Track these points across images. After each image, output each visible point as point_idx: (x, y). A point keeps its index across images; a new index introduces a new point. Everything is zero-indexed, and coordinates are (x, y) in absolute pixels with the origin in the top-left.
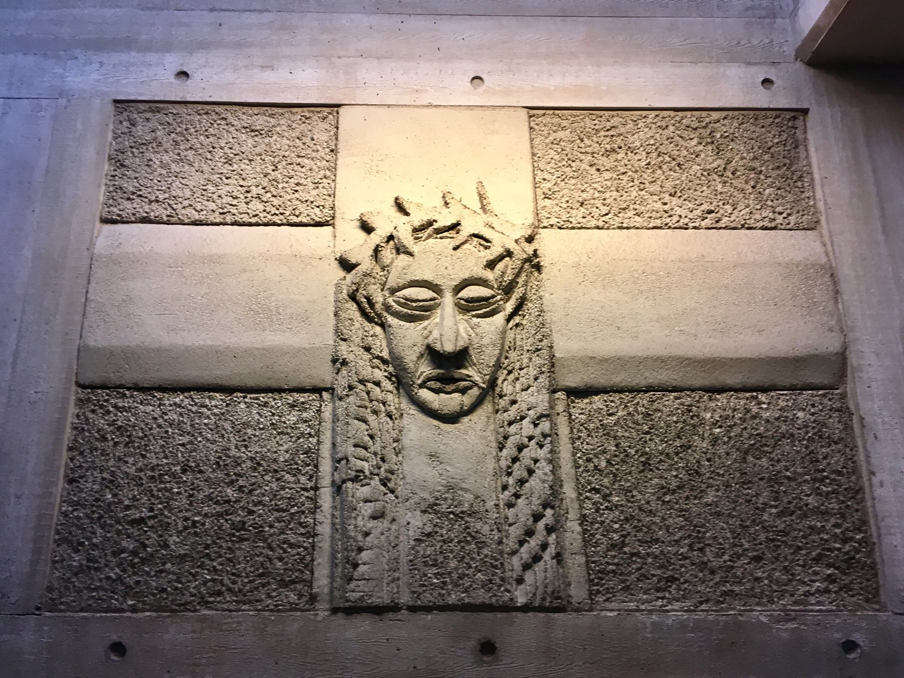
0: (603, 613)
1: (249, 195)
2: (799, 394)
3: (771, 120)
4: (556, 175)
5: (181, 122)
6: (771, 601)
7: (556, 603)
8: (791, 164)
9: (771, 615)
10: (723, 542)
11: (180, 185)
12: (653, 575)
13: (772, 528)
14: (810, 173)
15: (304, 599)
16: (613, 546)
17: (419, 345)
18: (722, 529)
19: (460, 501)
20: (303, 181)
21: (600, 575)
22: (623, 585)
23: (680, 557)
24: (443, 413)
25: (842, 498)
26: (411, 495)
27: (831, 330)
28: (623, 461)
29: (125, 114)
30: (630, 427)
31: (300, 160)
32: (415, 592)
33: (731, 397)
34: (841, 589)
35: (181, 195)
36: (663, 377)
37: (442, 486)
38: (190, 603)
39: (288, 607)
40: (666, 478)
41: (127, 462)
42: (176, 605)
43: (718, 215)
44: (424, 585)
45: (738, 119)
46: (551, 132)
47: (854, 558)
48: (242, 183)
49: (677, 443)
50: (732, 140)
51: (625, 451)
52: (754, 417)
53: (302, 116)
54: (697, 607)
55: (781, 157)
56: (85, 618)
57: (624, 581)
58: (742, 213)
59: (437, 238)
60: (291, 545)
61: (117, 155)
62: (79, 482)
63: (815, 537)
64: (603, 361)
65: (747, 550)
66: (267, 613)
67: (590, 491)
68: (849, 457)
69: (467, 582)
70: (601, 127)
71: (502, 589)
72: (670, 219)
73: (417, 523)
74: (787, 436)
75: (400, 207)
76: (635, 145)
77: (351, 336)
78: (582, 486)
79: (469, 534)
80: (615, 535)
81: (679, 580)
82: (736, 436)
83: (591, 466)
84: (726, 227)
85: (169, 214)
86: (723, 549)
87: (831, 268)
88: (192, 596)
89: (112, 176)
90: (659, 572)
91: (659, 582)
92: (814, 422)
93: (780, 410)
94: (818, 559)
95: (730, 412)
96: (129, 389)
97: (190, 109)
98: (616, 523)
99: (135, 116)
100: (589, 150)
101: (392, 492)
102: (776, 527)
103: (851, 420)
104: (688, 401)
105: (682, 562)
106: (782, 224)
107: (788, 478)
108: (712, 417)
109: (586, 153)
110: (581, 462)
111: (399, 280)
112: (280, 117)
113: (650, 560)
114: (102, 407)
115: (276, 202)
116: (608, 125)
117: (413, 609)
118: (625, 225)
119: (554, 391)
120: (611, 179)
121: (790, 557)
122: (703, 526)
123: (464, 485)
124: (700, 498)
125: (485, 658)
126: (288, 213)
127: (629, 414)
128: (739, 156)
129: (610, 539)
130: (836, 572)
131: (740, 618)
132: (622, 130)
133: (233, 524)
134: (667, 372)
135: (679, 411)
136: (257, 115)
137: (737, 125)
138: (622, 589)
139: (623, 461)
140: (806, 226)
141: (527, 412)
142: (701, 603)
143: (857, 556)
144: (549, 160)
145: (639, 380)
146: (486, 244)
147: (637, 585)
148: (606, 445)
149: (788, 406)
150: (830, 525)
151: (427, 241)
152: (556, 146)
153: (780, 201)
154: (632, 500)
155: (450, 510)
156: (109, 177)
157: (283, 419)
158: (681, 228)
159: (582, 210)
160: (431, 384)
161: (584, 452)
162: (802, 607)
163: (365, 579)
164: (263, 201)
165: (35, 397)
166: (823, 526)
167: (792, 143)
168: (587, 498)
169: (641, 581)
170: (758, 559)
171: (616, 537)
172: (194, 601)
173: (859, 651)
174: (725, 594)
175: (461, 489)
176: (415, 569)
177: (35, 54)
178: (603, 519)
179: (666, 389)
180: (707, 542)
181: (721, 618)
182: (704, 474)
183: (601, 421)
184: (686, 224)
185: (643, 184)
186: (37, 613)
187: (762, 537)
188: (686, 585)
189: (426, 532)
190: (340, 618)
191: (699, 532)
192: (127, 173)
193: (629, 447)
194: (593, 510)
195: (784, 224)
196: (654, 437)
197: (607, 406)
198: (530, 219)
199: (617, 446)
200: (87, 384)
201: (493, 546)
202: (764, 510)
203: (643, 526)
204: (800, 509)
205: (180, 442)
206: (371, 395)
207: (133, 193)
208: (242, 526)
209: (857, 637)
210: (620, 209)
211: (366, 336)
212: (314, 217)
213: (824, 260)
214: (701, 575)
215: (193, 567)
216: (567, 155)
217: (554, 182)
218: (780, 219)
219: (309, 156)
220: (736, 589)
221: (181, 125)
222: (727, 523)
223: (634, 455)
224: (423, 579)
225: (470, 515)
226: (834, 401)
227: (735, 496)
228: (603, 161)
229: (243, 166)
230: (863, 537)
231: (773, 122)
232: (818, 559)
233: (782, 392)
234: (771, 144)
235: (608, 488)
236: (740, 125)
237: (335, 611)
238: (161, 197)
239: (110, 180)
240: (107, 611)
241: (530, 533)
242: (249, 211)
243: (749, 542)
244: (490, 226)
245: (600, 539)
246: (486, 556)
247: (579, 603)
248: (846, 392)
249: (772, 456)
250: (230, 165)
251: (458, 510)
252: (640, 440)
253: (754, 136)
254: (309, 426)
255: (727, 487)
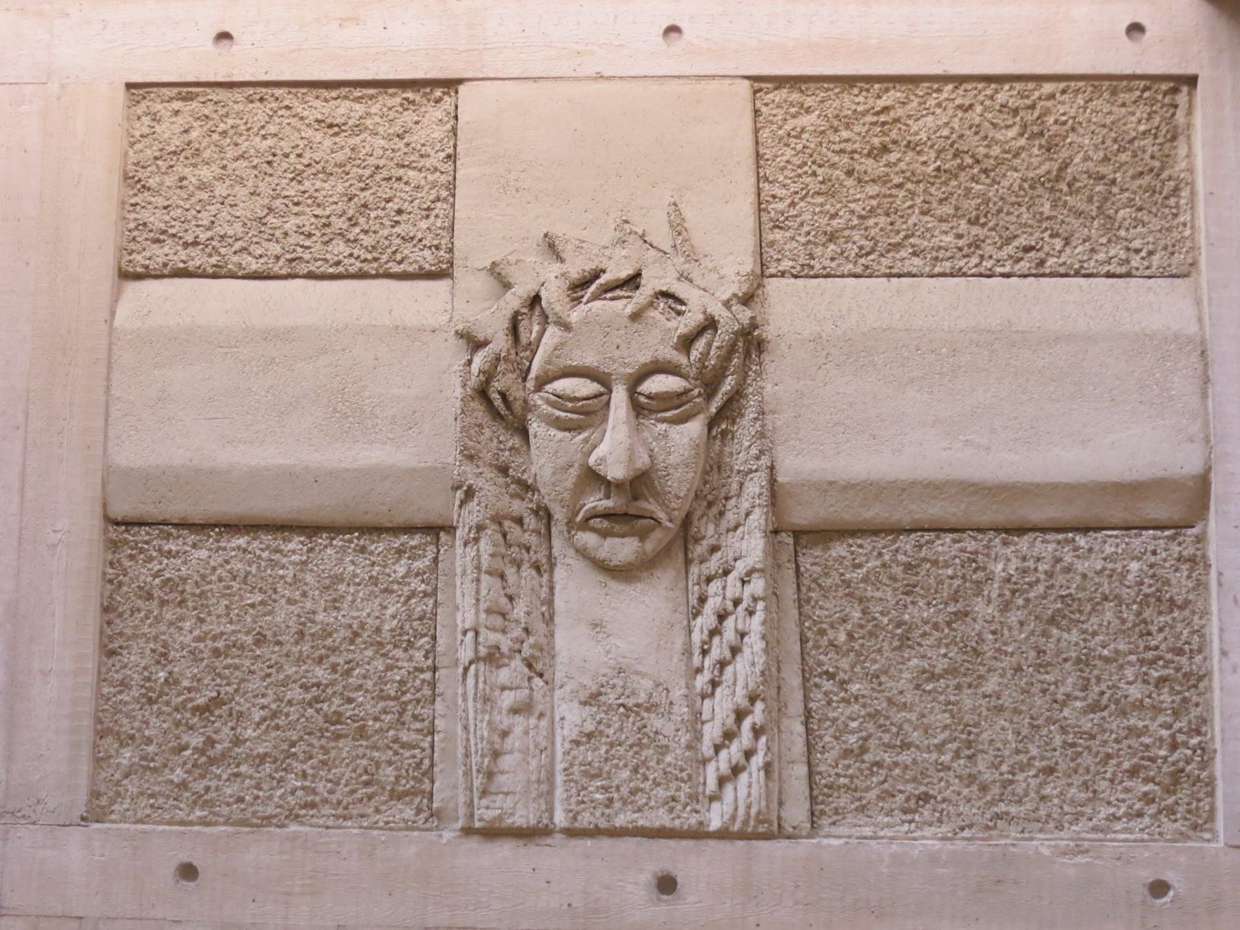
0: (825, 841)
1: (328, 230)
2: (1135, 535)
3: (1138, 93)
4: (792, 190)
5: (227, 115)
6: (1060, 827)
7: (762, 829)
8: (1162, 169)
9: (1055, 846)
10: (1002, 747)
11: (229, 218)
12: (901, 792)
13: (1073, 727)
14: (1192, 184)
15: (423, 816)
16: (847, 753)
17: (576, 465)
18: (1003, 729)
19: (634, 689)
20: (406, 206)
21: (826, 790)
22: (857, 804)
23: (940, 767)
24: (612, 564)
25: (1178, 688)
26: (565, 680)
27: (1191, 440)
28: (871, 634)
29: (144, 104)
30: (885, 584)
31: (401, 172)
32: (571, 811)
33: (1035, 539)
34: (1160, 812)
35: (230, 232)
36: (936, 510)
37: (610, 667)
38: (276, 816)
39: (402, 825)
40: (930, 658)
41: (181, 629)
42: (258, 818)
43: (1041, 255)
44: (583, 802)
45: (1085, 92)
46: (788, 117)
47: (1182, 771)
48: (318, 212)
49: (951, 609)
50: (1073, 129)
51: (875, 619)
52: (1068, 570)
53: (404, 99)
54: (956, 834)
55: (1147, 157)
56: (144, 832)
57: (860, 799)
58: (1077, 251)
59: (605, 299)
60: (404, 746)
61: (137, 171)
62: (121, 654)
63: (1133, 742)
64: (848, 487)
65: (1034, 758)
66: (375, 833)
67: (820, 676)
68: (1196, 628)
69: (641, 799)
70: (867, 107)
71: (688, 808)
72: (965, 260)
73: (574, 719)
74: (1111, 597)
75: (552, 248)
76: (918, 138)
77: (480, 451)
78: (810, 669)
79: (646, 734)
80: (851, 737)
81: (935, 798)
82: (1036, 597)
83: (824, 641)
84: (1051, 273)
85: (215, 263)
86: (1001, 756)
87: (1203, 342)
88: (278, 807)
89: (132, 205)
90: (909, 787)
91: (908, 800)
92: (1154, 576)
93: (1105, 559)
94: (1133, 772)
95: (1031, 564)
96: (176, 525)
97: (238, 95)
98: (854, 720)
99: (159, 107)
100: (849, 147)
101: (541, 675)
102: (1080, 727)
103: (1208, 574)
104: (971, 545)
105: (941, 774)
106: (1137, 269)
107: (1107, 660)
108: (1004, 570)
109: (842, 151)
110: (809, 634)
111: (549, 367)
112: (369, 102)
113: (897, 771)
114: (142, 551)
115: (368, 240)
116: (881, 103)
117: (571, 833)
118: (894, 271)
119: (776, 532)
120: (878, 195)
121: (1092, 768)
122: (977, 725)
123: (640, 668)
124: (976, 687)
125: (665, 897)
126: (384, 258)
127: (884, 565)
128: (1080, 155)
129: (844, 742)
130: (1157, 788)
131: (1013, 849)
132: (900, 112)
133: (326, 716)
134: (942, 503)
135: (957, 561)
136: (336, 99)
137: (1082, 102)
138: (856, 809)
139: (871, 634)
140: (1174, 271)
141: (733, 563)
142: (962, 829)
143: (1189, 768)
144: (782, 164)
145: (901, 515)
146: (679, 307)
147: (877, 805)
148: (848, 609)
149: (1117, 553)
150: (1156, 724)
151: (589, 305)
152: (795, 141)
153: (1139, 229)
154: (880, 688)
155: (621, 701)
156: (128, 207)
157: (387, 571)
158: (981, 275)
159: (832, 247)
160: (595, 522)
161: (814, 620)
162: (1101, 835)
163: (503, 793)
164: (349, 240)
165: (53, 538)
166: (1146, 727)
167: (1167, 132)
168: (816, 685)
169: (883, 799)
170: (1050, 771)
171: (852, 739)
172: (281, 814)
173: (1171, 893)
174: (998, 816)
175: (637, 673)
176: (571, 781)
177: (8, 10)
178: (835, 714)
179: (940, 529)
180: (980, 747)
181: (985, 849)
182: (985, 653)
183: (843, 575)
184: (990, 270)
185: (928, 203)
186: (83, 823)
187: (1058, 740)
188: (944, 806)
189: (587, 732)
190: (474, 843)
191: (969, 733)
192: (153, 199)
193: (882, 613)
194: (823, 703)
195: (1141, 267)
196: (919, 599)
197: (852, 553)
198: (748, 264)
199: (864, 612)
200: (120, 519)
201: (678, 751)
202: (1064, 704)
203: (892, 724)
204: (1117, 702)
205: (249, 602)
206: (508, 537)
207: (164, 232)
208: (337, 718)
209: (1169, 876)
210: (890, 244)
211: (502, 450)
212: (422, 263)
213: (1193, 329)
214: (966, 792)
215: (276, 771)
216: (811, 156)
217: (789, 201)
218: (1136, 261)
219: (414, 165)
220: (1013, 810)
221: (225, 119)
222: (1011, 722)
223: (887, 625)
224: (582, 793)
225: (648, 710)
226: (1184, 545)
227: (1027, 683)
228: (868, 165)
229: (318, 184)
230: (1200, 743)
231: (1140, 97)
232: (1133, 772)
233: (1110, 533)
234: (1134, 134)
235: (845, 672)
236: (1087, 102)
237: (468, 831)
238: (203, 237)
239: (129, 211)
240: (170, 823)
241: (729, 736)
242: (328, 256)
243: (1039, 747)
244: (686, 278)
245: (828, 743)
246: (669, 765)
247: (794, 828)
248: (1204, 532)
249: (1084, 626)
250: (300, 182)
251: (630, 702)
252: (897, 603)
253: (1108, 122)
254: (423, 581)
255: (1016, 670)
